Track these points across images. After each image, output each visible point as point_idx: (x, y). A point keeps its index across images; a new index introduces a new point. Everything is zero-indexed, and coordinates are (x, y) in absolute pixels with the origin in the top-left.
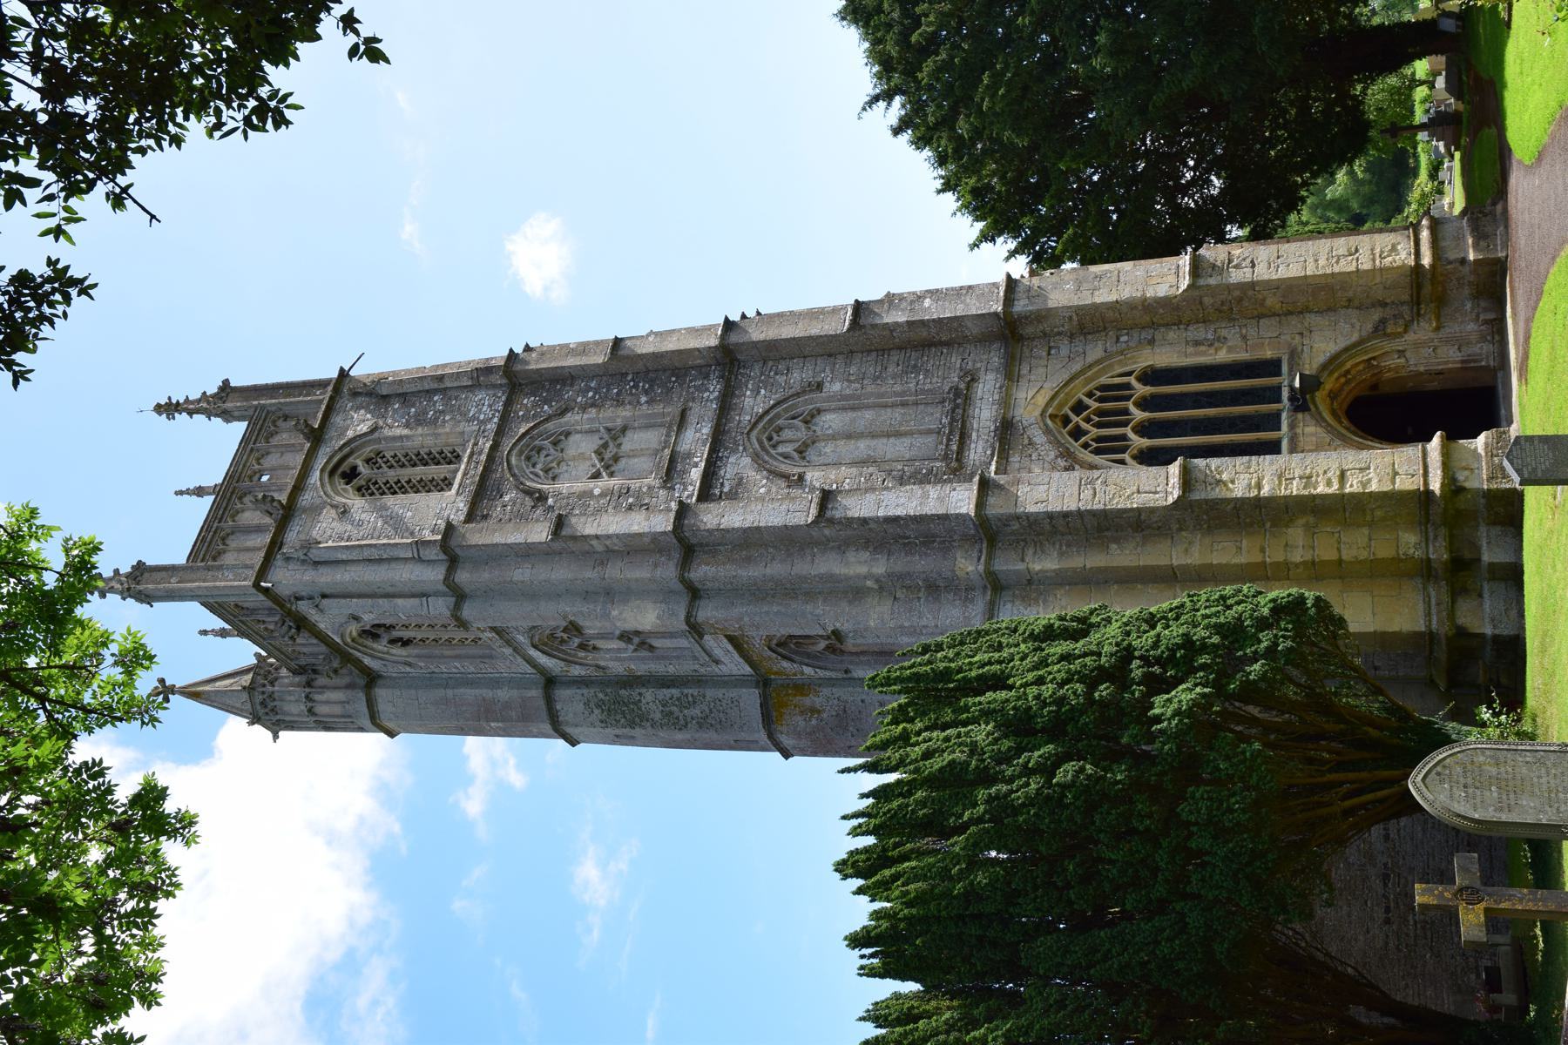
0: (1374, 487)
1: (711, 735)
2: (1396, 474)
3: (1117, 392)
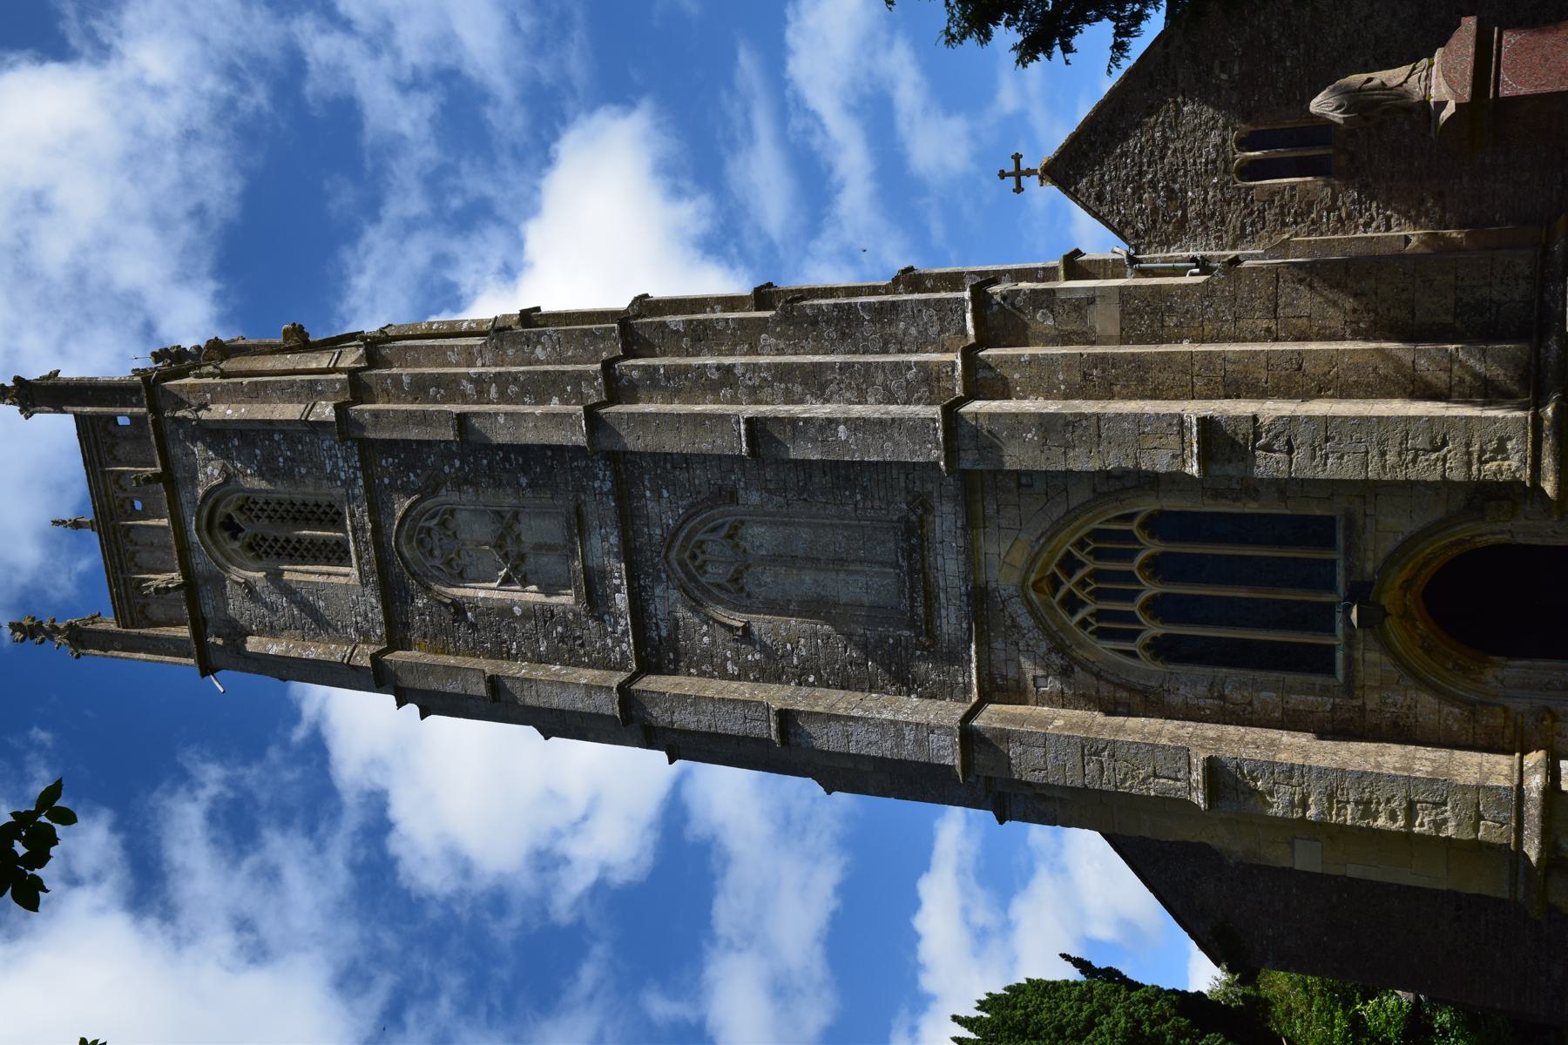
0: (1450, 831)
2: (1480, 817)
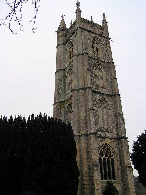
1: (57, 94)
3: (110, 154)
